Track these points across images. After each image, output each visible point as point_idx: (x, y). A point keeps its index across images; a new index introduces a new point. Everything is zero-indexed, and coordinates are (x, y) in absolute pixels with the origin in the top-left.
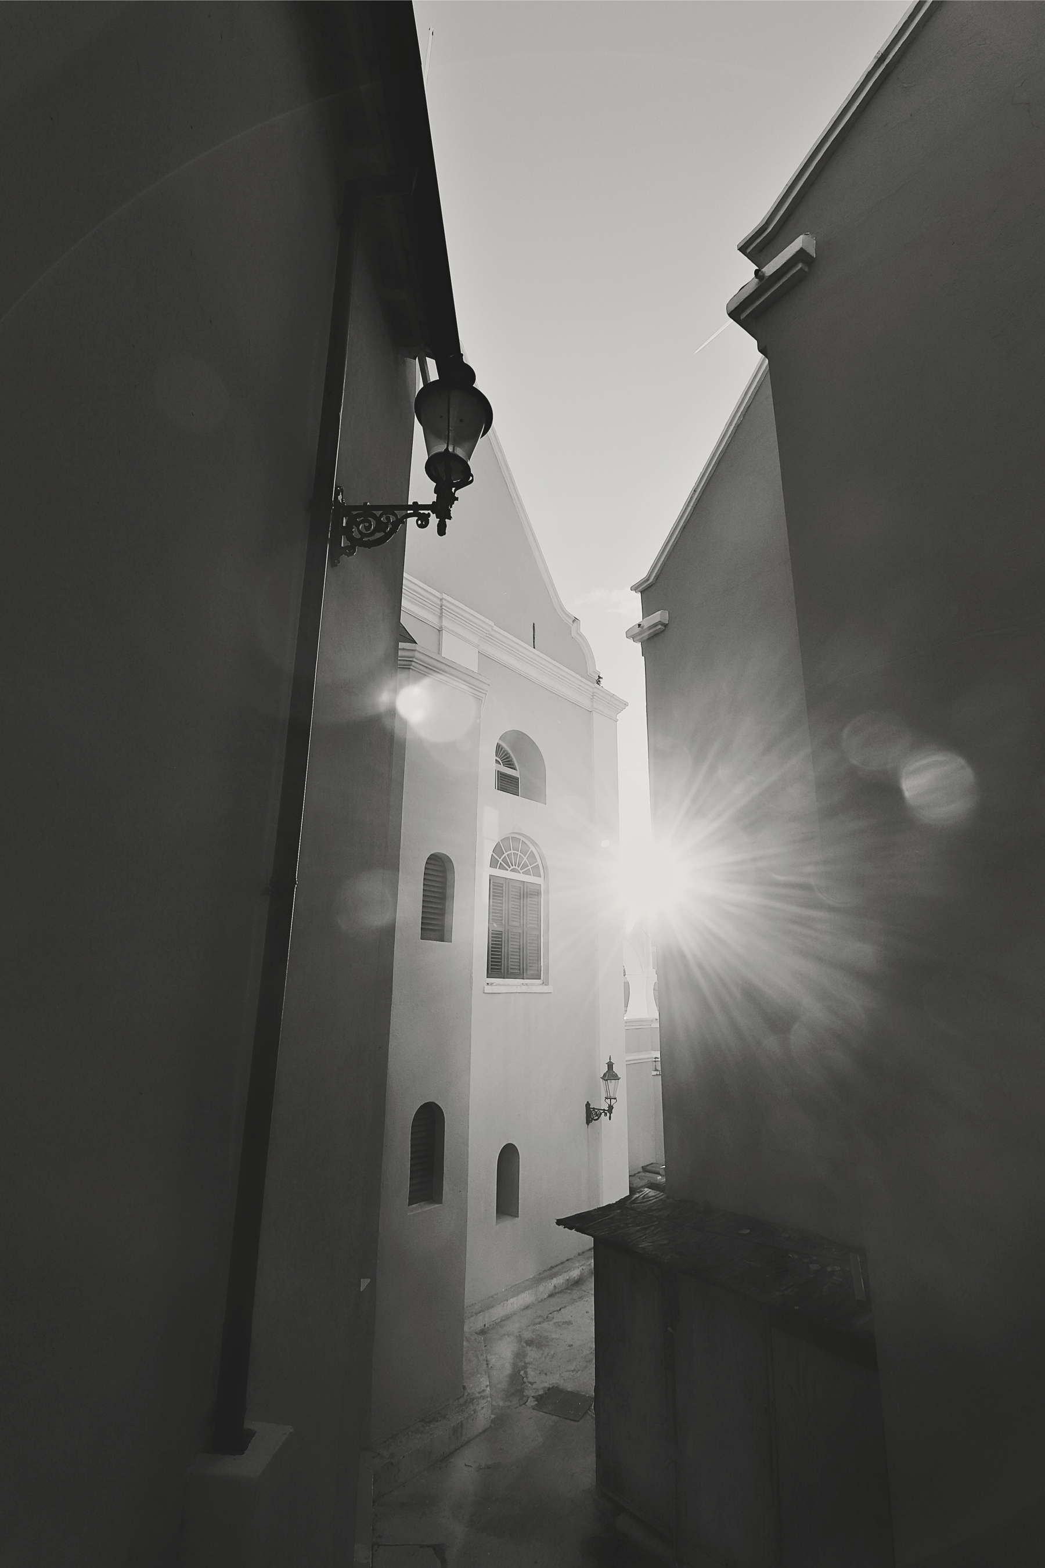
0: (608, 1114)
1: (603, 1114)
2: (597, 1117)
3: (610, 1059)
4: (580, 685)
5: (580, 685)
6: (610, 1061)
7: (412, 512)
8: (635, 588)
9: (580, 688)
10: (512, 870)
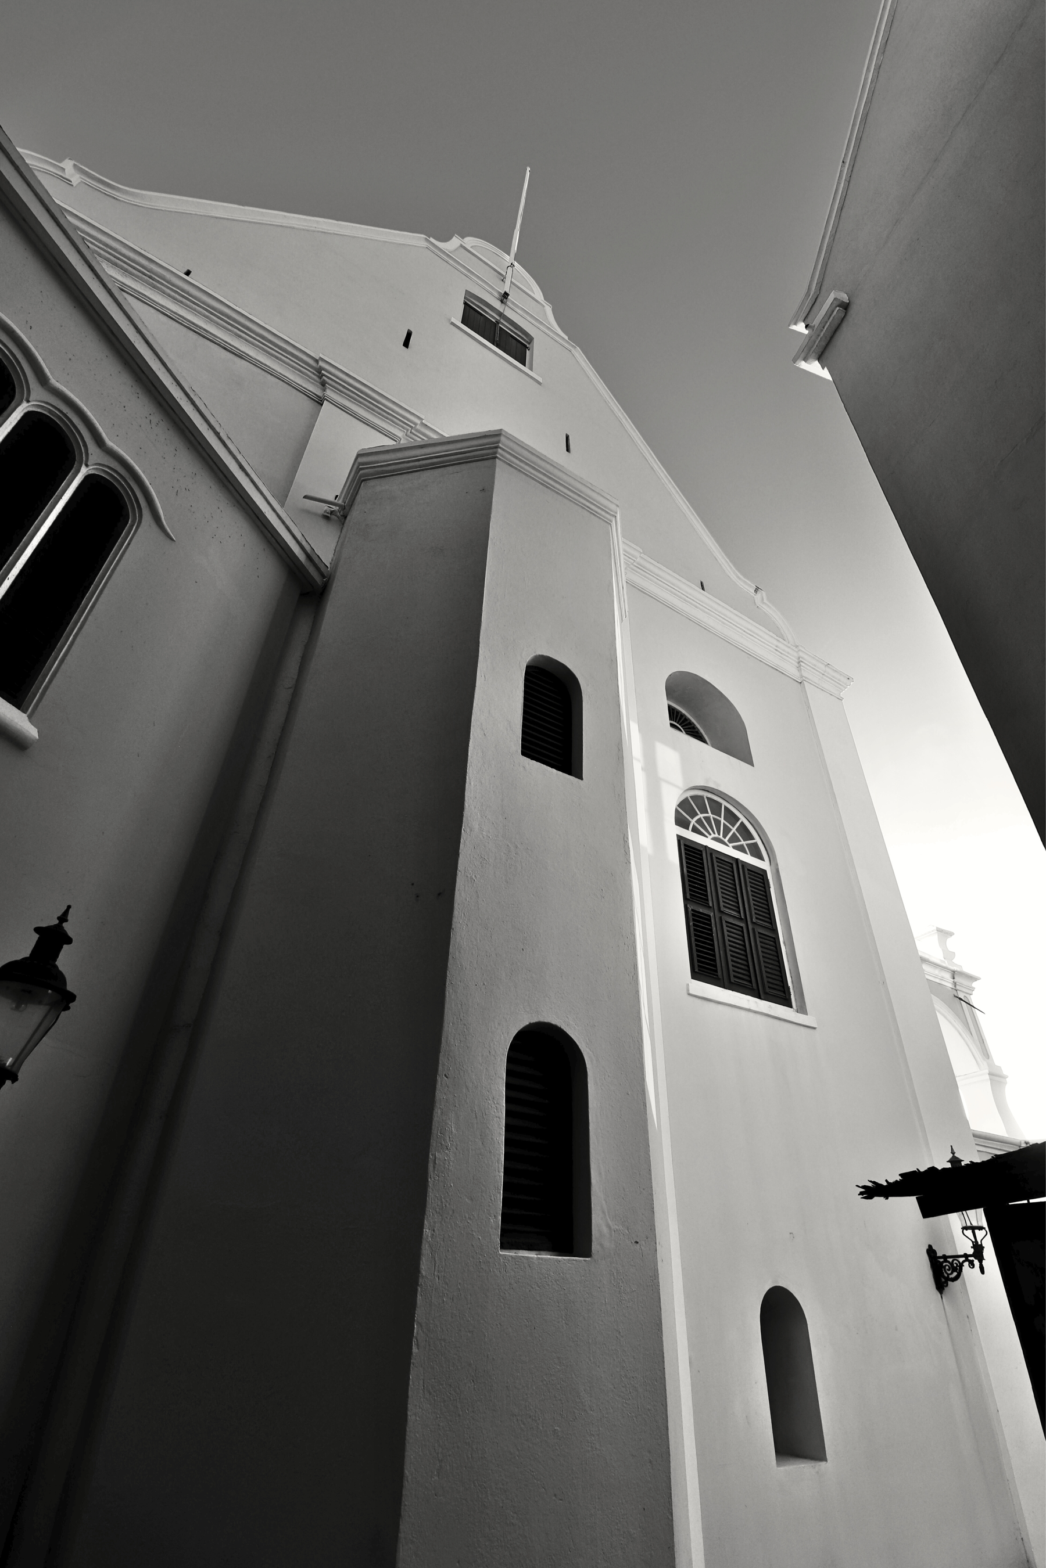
0: (976, 1263)
1: (966, 1264)
2: (955, 1274)
3: (953, 1153)
4: (777, 646)
5: (777, 646)
6: (954, 1157)
7: (529, 169)
8: (37, 930)
9: (778, 649)
10: (714, 839)
